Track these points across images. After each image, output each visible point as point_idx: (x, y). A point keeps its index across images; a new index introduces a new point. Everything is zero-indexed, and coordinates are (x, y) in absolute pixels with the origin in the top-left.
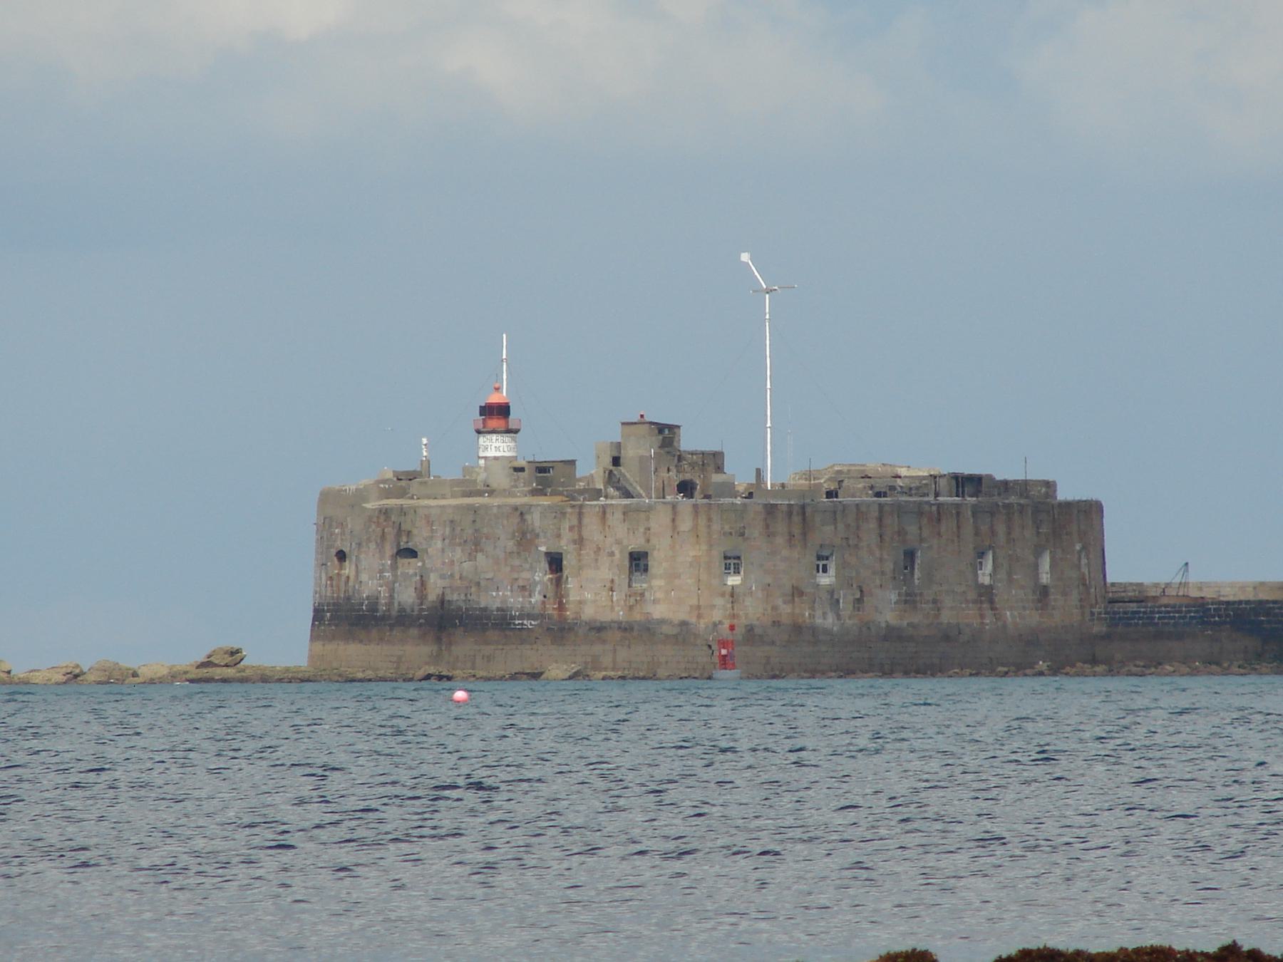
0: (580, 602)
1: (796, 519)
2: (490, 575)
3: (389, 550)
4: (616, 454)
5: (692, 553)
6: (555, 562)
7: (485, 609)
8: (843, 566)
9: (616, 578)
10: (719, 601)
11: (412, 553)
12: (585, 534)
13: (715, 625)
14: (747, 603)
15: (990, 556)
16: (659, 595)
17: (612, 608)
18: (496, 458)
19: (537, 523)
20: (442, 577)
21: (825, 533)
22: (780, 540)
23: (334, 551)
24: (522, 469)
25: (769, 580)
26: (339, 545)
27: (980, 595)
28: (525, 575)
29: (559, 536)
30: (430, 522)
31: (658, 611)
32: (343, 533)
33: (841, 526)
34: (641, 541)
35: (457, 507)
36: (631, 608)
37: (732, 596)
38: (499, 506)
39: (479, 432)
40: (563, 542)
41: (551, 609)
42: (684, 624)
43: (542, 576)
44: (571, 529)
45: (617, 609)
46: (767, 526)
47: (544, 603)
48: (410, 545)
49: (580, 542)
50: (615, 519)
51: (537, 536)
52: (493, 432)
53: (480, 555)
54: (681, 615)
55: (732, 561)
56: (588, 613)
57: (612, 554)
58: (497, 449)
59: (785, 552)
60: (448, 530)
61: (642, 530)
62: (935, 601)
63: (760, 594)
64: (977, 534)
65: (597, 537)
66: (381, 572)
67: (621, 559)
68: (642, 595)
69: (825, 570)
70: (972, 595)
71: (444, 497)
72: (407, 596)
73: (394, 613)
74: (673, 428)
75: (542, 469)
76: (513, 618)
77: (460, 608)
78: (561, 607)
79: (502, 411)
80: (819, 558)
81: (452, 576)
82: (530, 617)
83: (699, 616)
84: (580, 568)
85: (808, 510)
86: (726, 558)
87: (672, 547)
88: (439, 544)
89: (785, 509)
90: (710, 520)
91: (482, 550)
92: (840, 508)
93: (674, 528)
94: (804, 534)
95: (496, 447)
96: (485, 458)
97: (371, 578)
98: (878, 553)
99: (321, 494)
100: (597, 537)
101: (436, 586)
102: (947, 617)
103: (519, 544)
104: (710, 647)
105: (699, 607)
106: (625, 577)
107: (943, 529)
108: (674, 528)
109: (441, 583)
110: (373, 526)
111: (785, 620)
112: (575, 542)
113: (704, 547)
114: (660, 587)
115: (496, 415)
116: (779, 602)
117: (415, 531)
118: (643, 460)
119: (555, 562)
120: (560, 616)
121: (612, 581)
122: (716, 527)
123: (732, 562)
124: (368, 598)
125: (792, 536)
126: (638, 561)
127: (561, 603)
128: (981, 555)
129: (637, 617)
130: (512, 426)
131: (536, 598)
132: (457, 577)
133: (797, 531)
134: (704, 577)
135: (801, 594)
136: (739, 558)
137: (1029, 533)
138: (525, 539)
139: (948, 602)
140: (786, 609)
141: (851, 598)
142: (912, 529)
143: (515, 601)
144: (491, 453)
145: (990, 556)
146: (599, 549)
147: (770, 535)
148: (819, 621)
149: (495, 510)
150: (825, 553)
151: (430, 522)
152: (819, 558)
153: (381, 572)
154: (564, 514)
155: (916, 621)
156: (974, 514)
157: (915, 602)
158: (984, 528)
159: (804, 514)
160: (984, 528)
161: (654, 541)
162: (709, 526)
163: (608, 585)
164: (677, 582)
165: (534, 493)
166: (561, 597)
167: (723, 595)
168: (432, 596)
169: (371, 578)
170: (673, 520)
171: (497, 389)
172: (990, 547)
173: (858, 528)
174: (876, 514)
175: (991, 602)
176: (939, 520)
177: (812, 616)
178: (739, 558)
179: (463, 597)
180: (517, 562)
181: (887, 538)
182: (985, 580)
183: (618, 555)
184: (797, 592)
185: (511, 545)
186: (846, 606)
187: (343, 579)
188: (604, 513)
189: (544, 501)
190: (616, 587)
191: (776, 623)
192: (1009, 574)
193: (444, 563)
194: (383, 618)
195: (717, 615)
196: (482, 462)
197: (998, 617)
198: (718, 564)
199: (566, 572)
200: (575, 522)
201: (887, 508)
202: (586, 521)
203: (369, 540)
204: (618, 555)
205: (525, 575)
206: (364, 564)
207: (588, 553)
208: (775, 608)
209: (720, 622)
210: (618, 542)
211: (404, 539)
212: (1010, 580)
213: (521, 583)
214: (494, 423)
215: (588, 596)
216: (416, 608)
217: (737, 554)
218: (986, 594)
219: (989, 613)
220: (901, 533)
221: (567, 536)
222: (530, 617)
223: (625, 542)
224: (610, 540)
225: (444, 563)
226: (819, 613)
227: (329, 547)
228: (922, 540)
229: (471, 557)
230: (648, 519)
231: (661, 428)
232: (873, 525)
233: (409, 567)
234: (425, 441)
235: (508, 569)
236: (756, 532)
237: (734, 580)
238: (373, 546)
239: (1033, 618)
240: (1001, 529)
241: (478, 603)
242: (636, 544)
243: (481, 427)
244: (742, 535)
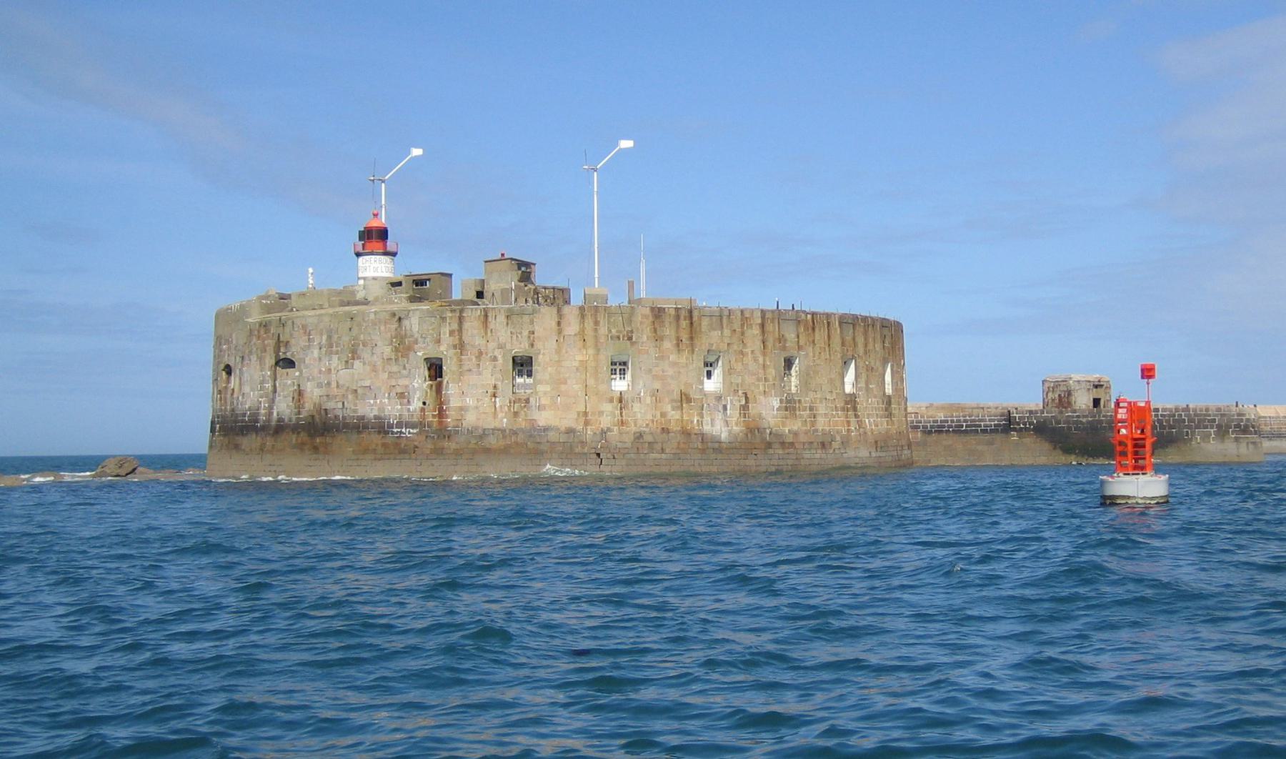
0: (461, 409)
1: (684, 323)
2: (367, 383)
3: (270, 360)
4: (479, 289)
5: (579, 358)
6: (436, 369)
7: (363, 418)
8: (729, 372)
9: (499, 383)
10: (608, 407)
11: (290, 363)
12: (466, 339)
13: (603, 432)
14: (636, 409)
15: (853, 365)
16: (544, 401)
17: (495, 413)
18: (374, 279)
19: (416, 328)
20: (320, 385)
21: (712, 338)
22: (668, 345)
23: (222, 366)
24: (399, 284)
25: (657, 385)
26: (226, 360)
27: (847, 403)
28: (403, 382)
29: (438, 341)
30: (306, 331)
31: (544, 418)
32: (229, 349)
33: (727, 332)
34: (526, 345)
35: (334, 315)
36: (516, 414)
37: (621, 401)
38: (375, 313)
39: (358, 255)
40: (443, 348)
41: (430, 417)
42: (570, 431)
43: (419, 382)
44: (451, 333)
45: (500, 415)
46: (655, 331)
47: (423, 410)
48: (289, 355)
49: (461, 347)
50: (498, 322)
51: (416, 342)
52: (372, 254)
53: (357, 363)
54: (568, 420)
55: (618, 367)
56: (470, 419)
57: (495, 359)
58: (376, 270)
59: (673, 357)
60: (324, 337)
61: (526, 333)
62: (811, 409)
63: (648, 400)
64: (843, 344)
65: (479, 341)
66: (262, 382)
67: (505, 363)
68: (527, 401)
69: (709, 375)
70: (840, 404)
71: (321, 307)
72: (284, 408)
73: (273, 423)
74: (528, 265)
75: (420, 282)
76: (391, 426)
77: (336, 417)
78: (441, 414)
79: (383, 234)
80: (706, 365)
81: (329, 384)
82: (409, 425)
83: (587, 423)
84: (461, 374)
85: (695, 314)
86: (613, 363)
87: (558, 351)
88: (316, 352)
89: (673, 312)
90: (596, 323)
91: (359, 358)
92: (726, 313)
93: (560, 332)
94: (692, 338)
95: (375, 267)
96: (364, 279)
97: (252, 390)
98: (761, 360)
99: (217, 316)
100: (479, 341)
101: (313, 394)
102: (821, 424)
103: (397, 350)
104: (598, 455)
105: (586, 414)
106: (508, 382)
107: (817, 337)
108: (560, 332)
109: (317, 392)
110: (254, 340)
111: (674, 427)
112: (455, 347)
113: (591, 351)
114: (545, 393)
115: (375, 238)
116: (668, 408)
117: (293, 342)
118: (505, 293)
119: (436, 369)
120: (440, 423)
121: (495, 387)
122: (603, 330)
123: (619, 367)
124: (250, 409)
125: (679, 340)
126: (523, 365)
127: (441, 410)
128: (846, 364)
129: (521, 423)
130: (389, 249)
131: (416, 405)
132: (334, 385)
133: (685, 336)
134: (591, 382)
135: (689, 400)
136: (625, 364)
137: (878, 346)
138: (402, 347)
139: (821, 409)
140: (674, 415)
141: (738, 405)
142: (791, 336)
143: (392, 410)
144: (370, 274)
145: (853, 365)
146: (481, 353)
147: (658, 339)
148: (707, 428)
149: (372, 316)
150: (711, 359)
151: (306, 331)
152: (706, 365)
153: (262, 382)
154: (443, 319)
155: (795, 428)
156: (841, 323)
157: (794, 409)
158: (849, 338)
159: (691, 317)
160: (849, 338)
161: (538, 345)
162: (596, 330)
163: (491, 391)
164: (563, 387)
165: (413, 299)
166: (441, 403)
167: (611, 400)
168: (308, 406)
169: (252, 390)
170: (559, 324)
171: (376, 215)
172: (853, 357)
173: (743, 334)
174: (759, 321)
175: (855, 409)
176: (813, 329)
177: (700, 423)
178: (625, 364)
179: (340, 405)
180: (395, 368)
181: (770, 345)
182: (849, 389)
183: (500, 360)
184: (685, 398)
185: (388, 351)
186: (733, 413)
187: (229, 392)
188: (486, 316)
189: (424, 307)
190: (499, 392)
191: (665, 431)
192: (867, 384)
193: (320, 372)
194: (264, 428)
195: (605, 422)
196: (361, 282)
197: (860, 423)
198: (605, 368)
199: (446, 379)
200: (455, 326)
201: (768, 315)
202: (466, 325)
203: (251, 352)
204: (500, 360)
205: (403, 382)
206: (246, 376)
207: (470, 360)
208: (663, 415)
209: (609, 429)
210: (501, 347)
211: (282, 350)
212: (867, 389)
213: (399, 390)
214: (377, 245)
215: (470, 401)
216: (294, 418)
217: (624, 359)
218: (851, 401)
219: (853, 420)
220: (781, 339)
221: (447, 340)
222: (409, 425)
223: (508, 346)
224: (492, 345)
225: (320, 372)
226: (707, 419)
227: (219, 363)
228: (800, 348)
229: (348, 364)
230: (532, 322)
231: (521, 264)
232: (756, 331)
233: (288, 379)
234: (311, 270)
235: (386, 375)
236: (644, 336)
237: (620, 385)
238: (254, 358)
239: (883, 425)
240: (860, 340)
241: (355, 411)
242: (520, 348)
243: (360, 249)
244: (630, 339)
